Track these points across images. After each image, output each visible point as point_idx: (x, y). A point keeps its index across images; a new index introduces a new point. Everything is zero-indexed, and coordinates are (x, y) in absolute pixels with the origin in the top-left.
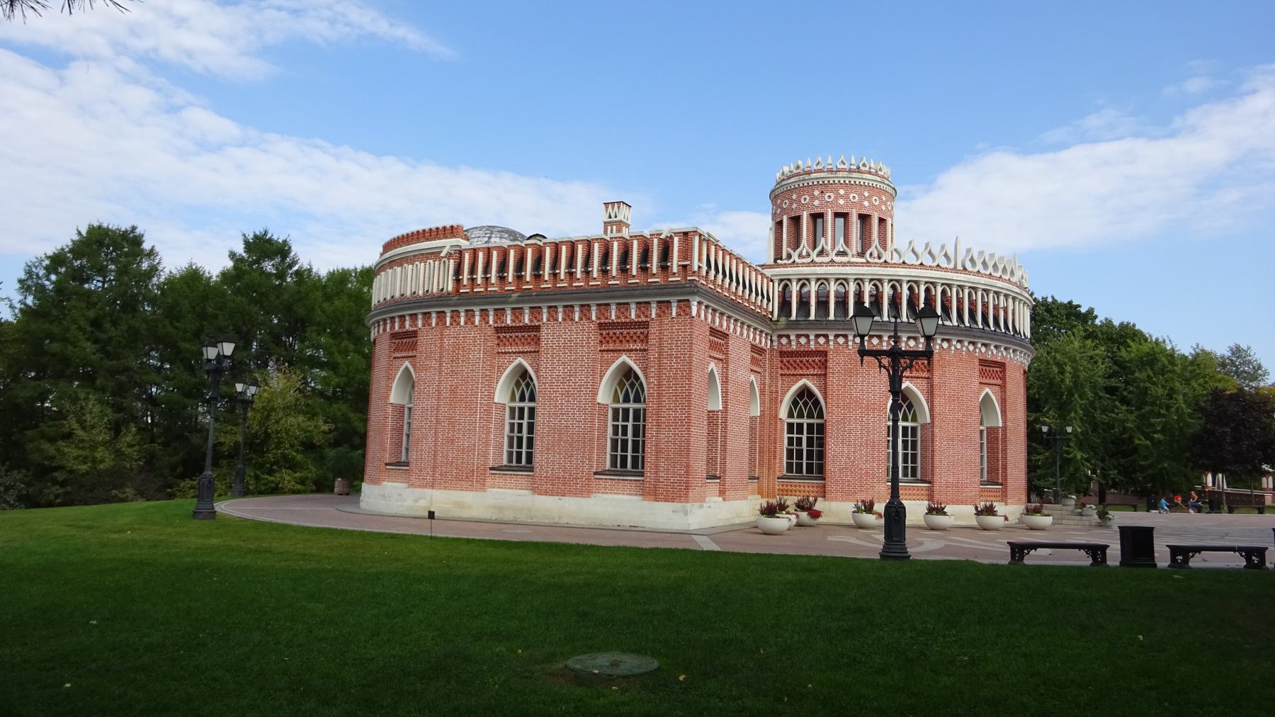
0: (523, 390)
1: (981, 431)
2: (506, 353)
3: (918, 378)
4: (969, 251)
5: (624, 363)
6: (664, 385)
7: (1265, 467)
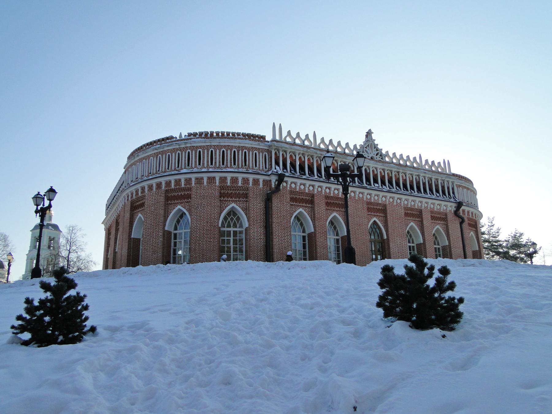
1: (304, 237)
4: (323, 139)
7: (446, 305)
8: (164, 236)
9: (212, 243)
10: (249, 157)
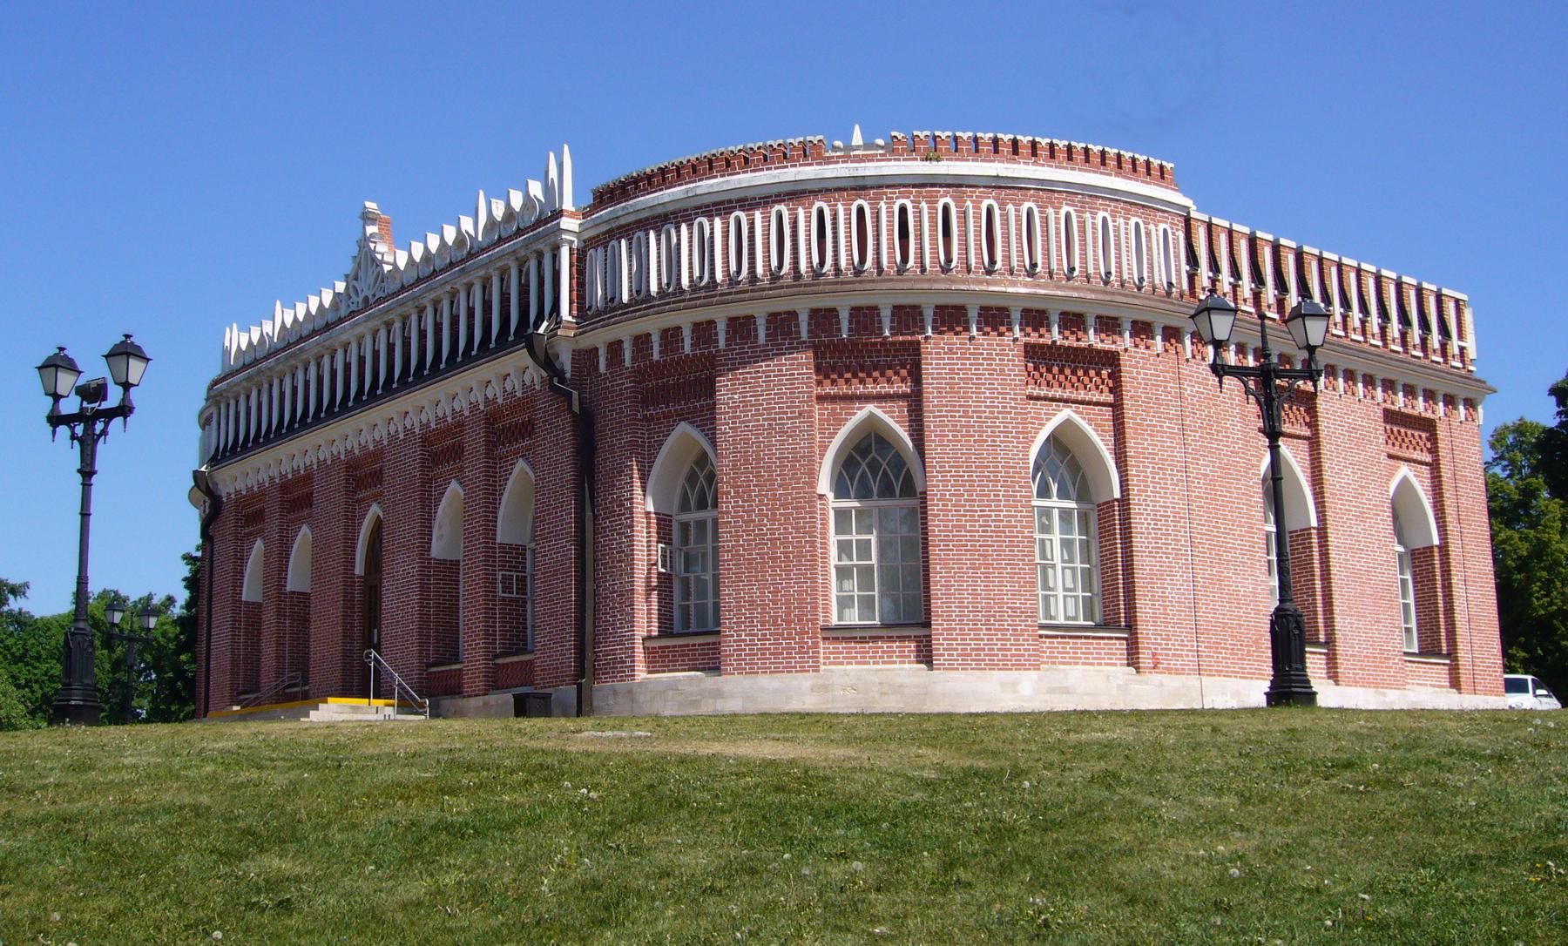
3: (1089, 403)
5: (872, 416)
6: (934, 477)
8: (424, 587)
9: (1004, 560)
10: (809, 249)
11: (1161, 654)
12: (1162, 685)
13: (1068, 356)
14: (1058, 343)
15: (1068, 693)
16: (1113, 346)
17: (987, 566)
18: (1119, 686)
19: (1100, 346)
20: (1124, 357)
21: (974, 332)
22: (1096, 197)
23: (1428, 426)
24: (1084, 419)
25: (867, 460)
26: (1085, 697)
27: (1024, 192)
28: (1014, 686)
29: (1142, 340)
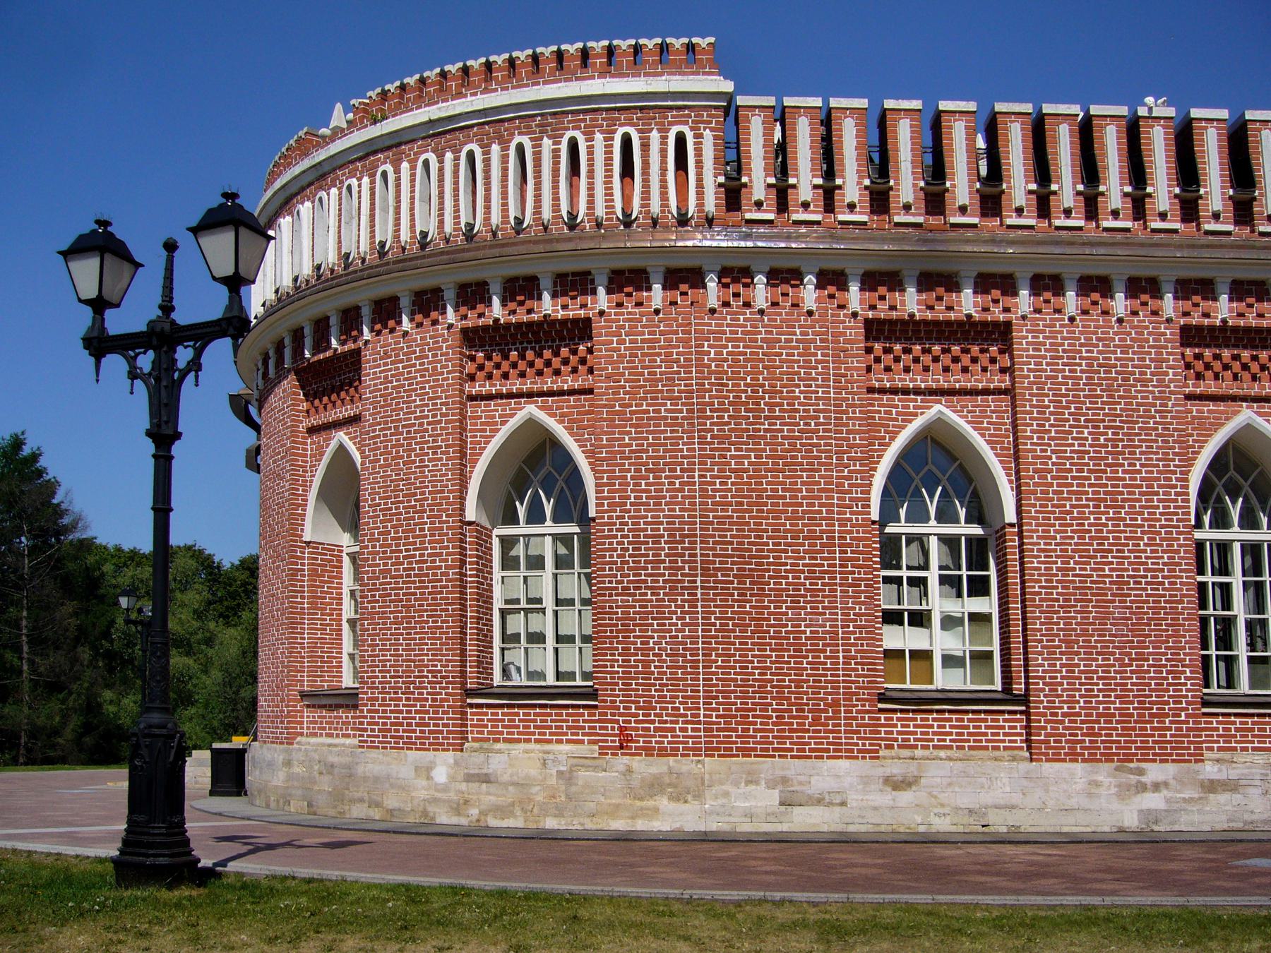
0: (536, 496)
2: (894, 391)
3: (561, 393)
11: (636, 729)
12: (629, 771)
13: (524, 335)
14: (1230, 323)
15: (488, 782)
16: (582, 312)
17: (409, 619)
18: (560, 773)
19: (561, 314)
20: (598, 325)
21: (406, 324)
22: (563, 113)
23: (1001, 334)
24: (552, 415)
25: (921, 474)
26: (511, 788)
27: (466, 132)
28: (425, 771)
29: (684, 294)
